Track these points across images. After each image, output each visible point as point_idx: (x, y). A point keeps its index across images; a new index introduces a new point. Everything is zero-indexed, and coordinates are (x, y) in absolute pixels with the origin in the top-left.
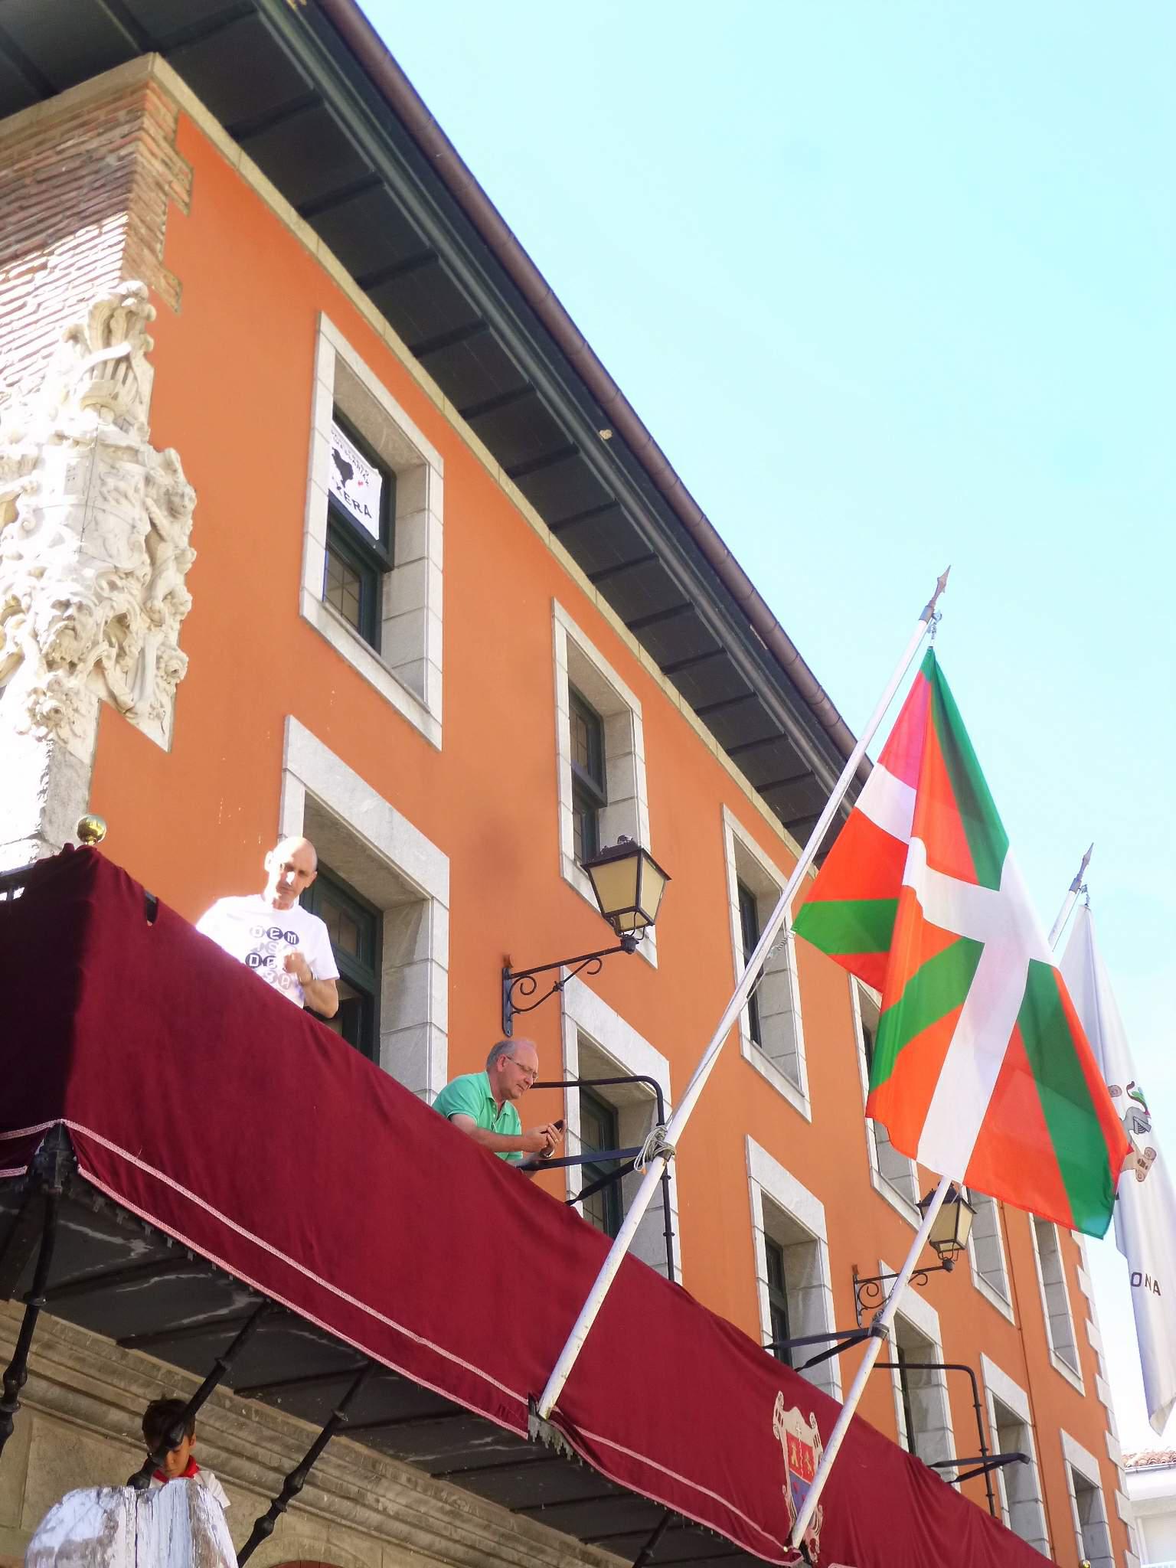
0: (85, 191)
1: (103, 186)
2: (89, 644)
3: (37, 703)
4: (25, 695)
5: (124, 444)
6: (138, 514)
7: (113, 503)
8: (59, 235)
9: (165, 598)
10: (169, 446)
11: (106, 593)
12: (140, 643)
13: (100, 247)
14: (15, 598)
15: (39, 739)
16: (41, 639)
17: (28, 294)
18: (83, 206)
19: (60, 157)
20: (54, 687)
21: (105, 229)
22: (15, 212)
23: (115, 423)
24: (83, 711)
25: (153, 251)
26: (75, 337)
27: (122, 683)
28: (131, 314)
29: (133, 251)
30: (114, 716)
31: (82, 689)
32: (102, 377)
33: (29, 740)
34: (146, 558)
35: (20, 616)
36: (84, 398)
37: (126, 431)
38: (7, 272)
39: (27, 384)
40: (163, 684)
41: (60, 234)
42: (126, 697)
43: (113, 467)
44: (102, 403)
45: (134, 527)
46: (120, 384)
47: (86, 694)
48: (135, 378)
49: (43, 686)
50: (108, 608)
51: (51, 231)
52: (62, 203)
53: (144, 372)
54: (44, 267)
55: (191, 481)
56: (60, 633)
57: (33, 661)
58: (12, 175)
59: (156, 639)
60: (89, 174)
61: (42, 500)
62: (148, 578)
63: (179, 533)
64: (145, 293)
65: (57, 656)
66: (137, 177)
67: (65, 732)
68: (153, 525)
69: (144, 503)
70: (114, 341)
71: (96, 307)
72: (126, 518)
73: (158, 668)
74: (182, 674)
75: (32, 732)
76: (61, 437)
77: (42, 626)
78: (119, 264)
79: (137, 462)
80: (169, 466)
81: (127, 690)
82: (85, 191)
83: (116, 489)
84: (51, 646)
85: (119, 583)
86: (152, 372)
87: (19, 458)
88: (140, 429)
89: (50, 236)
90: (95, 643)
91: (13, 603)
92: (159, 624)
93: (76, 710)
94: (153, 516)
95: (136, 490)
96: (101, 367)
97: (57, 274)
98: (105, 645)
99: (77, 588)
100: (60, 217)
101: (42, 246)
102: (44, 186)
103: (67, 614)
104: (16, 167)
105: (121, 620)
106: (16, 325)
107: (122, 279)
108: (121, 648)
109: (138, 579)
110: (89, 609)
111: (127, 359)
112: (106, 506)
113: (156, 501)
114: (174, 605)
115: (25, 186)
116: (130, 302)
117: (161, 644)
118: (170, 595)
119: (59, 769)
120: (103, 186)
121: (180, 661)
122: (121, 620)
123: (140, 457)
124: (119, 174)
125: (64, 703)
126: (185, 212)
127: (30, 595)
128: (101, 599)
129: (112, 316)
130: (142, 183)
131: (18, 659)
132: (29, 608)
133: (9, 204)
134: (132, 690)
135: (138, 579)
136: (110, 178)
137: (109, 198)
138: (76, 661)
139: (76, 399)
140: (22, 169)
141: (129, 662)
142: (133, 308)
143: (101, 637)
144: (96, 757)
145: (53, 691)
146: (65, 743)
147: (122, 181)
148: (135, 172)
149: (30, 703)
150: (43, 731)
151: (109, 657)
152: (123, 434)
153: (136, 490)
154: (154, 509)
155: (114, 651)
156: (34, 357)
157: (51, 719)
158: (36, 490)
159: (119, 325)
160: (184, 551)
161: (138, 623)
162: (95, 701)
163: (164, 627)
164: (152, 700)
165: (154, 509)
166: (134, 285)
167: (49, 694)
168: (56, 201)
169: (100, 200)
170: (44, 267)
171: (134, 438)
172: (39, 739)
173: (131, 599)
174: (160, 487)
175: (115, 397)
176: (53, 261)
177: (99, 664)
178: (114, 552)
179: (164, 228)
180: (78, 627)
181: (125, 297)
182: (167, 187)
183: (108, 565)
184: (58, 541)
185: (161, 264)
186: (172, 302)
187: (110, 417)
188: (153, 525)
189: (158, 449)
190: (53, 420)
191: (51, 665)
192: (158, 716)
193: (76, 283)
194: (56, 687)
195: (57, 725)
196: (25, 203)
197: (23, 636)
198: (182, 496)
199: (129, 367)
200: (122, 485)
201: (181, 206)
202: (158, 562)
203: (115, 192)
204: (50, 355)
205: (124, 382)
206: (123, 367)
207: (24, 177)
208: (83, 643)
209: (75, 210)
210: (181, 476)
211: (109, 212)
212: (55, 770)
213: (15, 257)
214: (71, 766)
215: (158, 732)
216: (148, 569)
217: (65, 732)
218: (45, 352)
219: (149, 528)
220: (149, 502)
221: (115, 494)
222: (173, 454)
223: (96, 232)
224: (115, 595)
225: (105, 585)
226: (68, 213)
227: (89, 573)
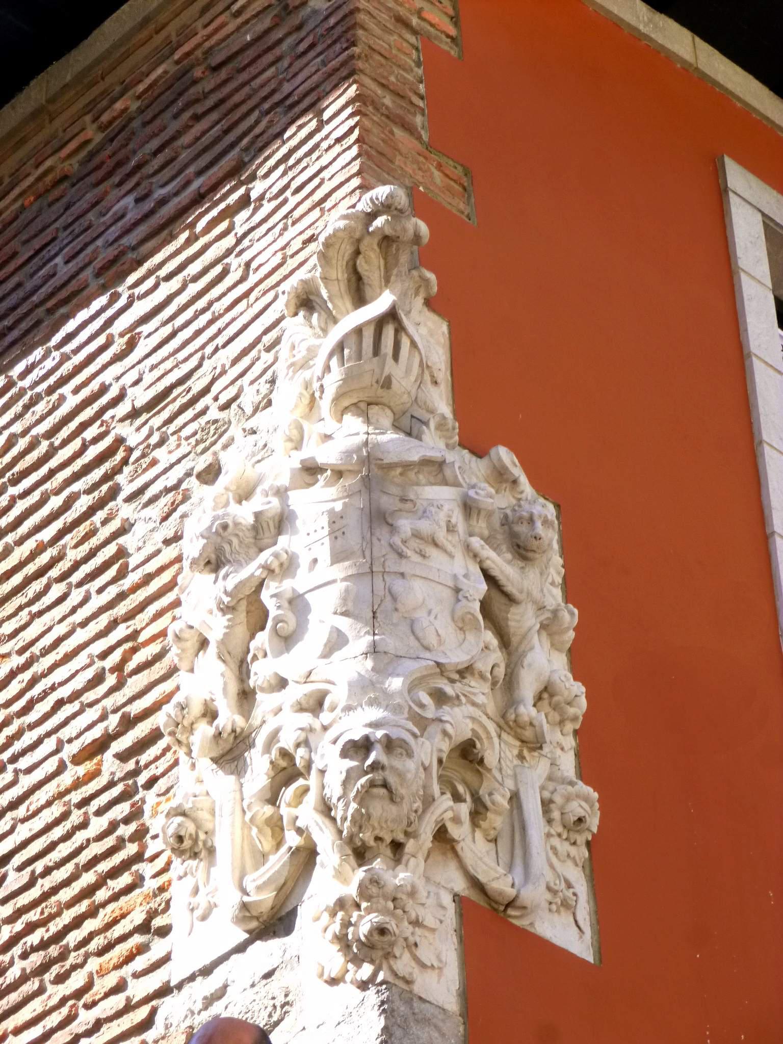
0: (285, 63)
1: (312, 46)
2: (418, 804)
3: (346, 924)
4: (326, 917)
5: (415, 457)
6: (460, 566)
7: (416, 558)
8: (261, 144)
9: (539, 698)
10: (495, 444)
11: (431, 712)
12: (510, 784)
13: (324, 145)
14: (284, 754)
15: (363, 986)
16: (338, 814)
17: (228, 252)
18: (287, 88)
19: (240, 20)
20: (371, 889)
21: (326, 115)
22: (187, 127)
23: (396, 427)
24: (430, 921)
25: (409, 129)
26: (306, 302)
27: (490, 860)
28: (386, 241)
29: (375, 139)
30: (487, 920)
31: (421, 884)
32: (359, 356)
33: (348, 992)
34: (490, 637)
35: (301, 782)
36: (337, 399)
37: (419, 438)
38: (192, 225)
39: (248, 400)
40: (564, 847)
41: (259, 144)
42: (501, 883)
43: (403, 500)
44: (362, 400)
45: (457, 590)
46: (390, 360)
47: (431, 892)
48: (413, 344)
49: (351, 891)
50: (439, 736)
51: (245, 141)
52: (256, 91)
53: (430, 334)
54: (245, 202)
55: (542, 488)
56: (364, 797)
57: (330, 853)
58: (173, 69)
59: (533, 778)
60: (289, 34)
61: (300, 582)
62: (501, 672)
63: (542, 585)
64: (402, 199)
65: (367, 836)
66: (361, 17)
67: (404, 964)
68: (490, 578)
69: (468, 548)
70: (368, 292)
71: (327, 245)
72: (441, 580)
73: (550, 821)
74: (594, 823)
75: (348, 977)
76: (312, 470)
77: (334, 790)
78: (355, 167)
79: (445, 482)
80: (501, 476)
81: (501, 870)
82: (285, 63)
83: (417, 535)
84: (354, 821)
85: (449, 690)
86: (444, 328)
87: (251, 520)
88: (441, 426)
89: (246, 149)
90: (428, 801)
91: (283, 763)
92: (535, 744)
93: (416, 923)
94: (488, 564)
95: (451, 529)
96: (353, 340)
97: (267, 207)
98: (446, 801)
99: (376, 714)
100: (256, 114)
101: (234, 172)
102: (223, 74)
103: (369, 762)
104: (176, 56)
105: (467, 753)
106: (218, 307)
107: (364, 187)
108: (477, 800)
109: (482, 676)
110: (403, 744)
111: (391, 316)
112: (404, 567)
113: (487, 540)
114: (555, 707)
115: (195, 82)
116: (379, 222)
117: (547, 776)
118: (546, 693)
119: (406, 1032)
120: (312, 46)
121: (584, 802)
122: (467, 753)
123: (448, 472)
124: (332, 21)
125: (393, 915)
126: (454, 52)
127: (306, 743)
128: (422, 723)
129: (357, 253)
130: (371, 25)
131: (306, 857)
132: (309, 765)
133: (176, 116)
134: (510, 868)
135: (482, 676)
136: (320, 31)
137: (324, 63)
138: (401, 837)
139: (325, 404)
140: (188, 54)
141: (496, 821)
142: (388, 231)
143: (436, 788)
144: (470, 994)
145: (369, 899)
146: (408, 982)
147: (339, 30)
148: (357, 10)
149: (336, 927)
150: (367, 970)
151: (456, 820)
152: (413, 442)
153: (451, 529)
154: (488, 553)
155: (464, 809)
156: (254, 353)
157: (374, 948)
158: (288, 567)
159: (371, 265)
160: (555, 612)
161: (498, 751)
162: (447, 900)
163: (546, 749)
164: (549, 876)
165: (488, 553)
166: (382, 192)
167: (364, 905)
168: (247, 89)
169: (312, 70)
170: (245, 202)
171: (433, 444)
172: (363, 986)
173: (477, 713)
174: (490, 514)
175: (387, 383)
176: (257, 188)
177: (441, 835)
178: (432, 640)
179: (422, 88)
180: (392, 780)
181: (372, 216)
182: (415, 21)
183: (425, 664)
184: (337, 642)
185: (429, 147)
186: (458, 205)
187: (386, 419)
188: (490, 578)
189: (479, 452)
190: (298, 446)
191: (361, 854)
192: (565, 904)
193: (296, 214)
194: (374, 890)
195: (388, 955)
196: (199, 109)
197: (308, 814)
198: (531, 520)
199: (400, 329)
200: (425, 526)
201: (445, 45)
202: (515, 640)
203: (331, 53)
204: (277, 342)
205: (396, 356)
206: (389, 331)
207: (192, 67)
208: (405, 807)
209: (277, 97)
210: (526, 487)
211: (327, 86)
212: (398, 1033)
213: (199, 198)
214: (426, 1021)
215: (570, 932)
216: (497, 656)
217: (404, 964)
218: (267, 339)
219: (483, 587)
220: (476, 542)
221: (414, 543)
222: (504, 454)
223: (313, 124)
224: (448, 713)
225: (425, 699)
226: (266, 106)
227: (396, 684)
